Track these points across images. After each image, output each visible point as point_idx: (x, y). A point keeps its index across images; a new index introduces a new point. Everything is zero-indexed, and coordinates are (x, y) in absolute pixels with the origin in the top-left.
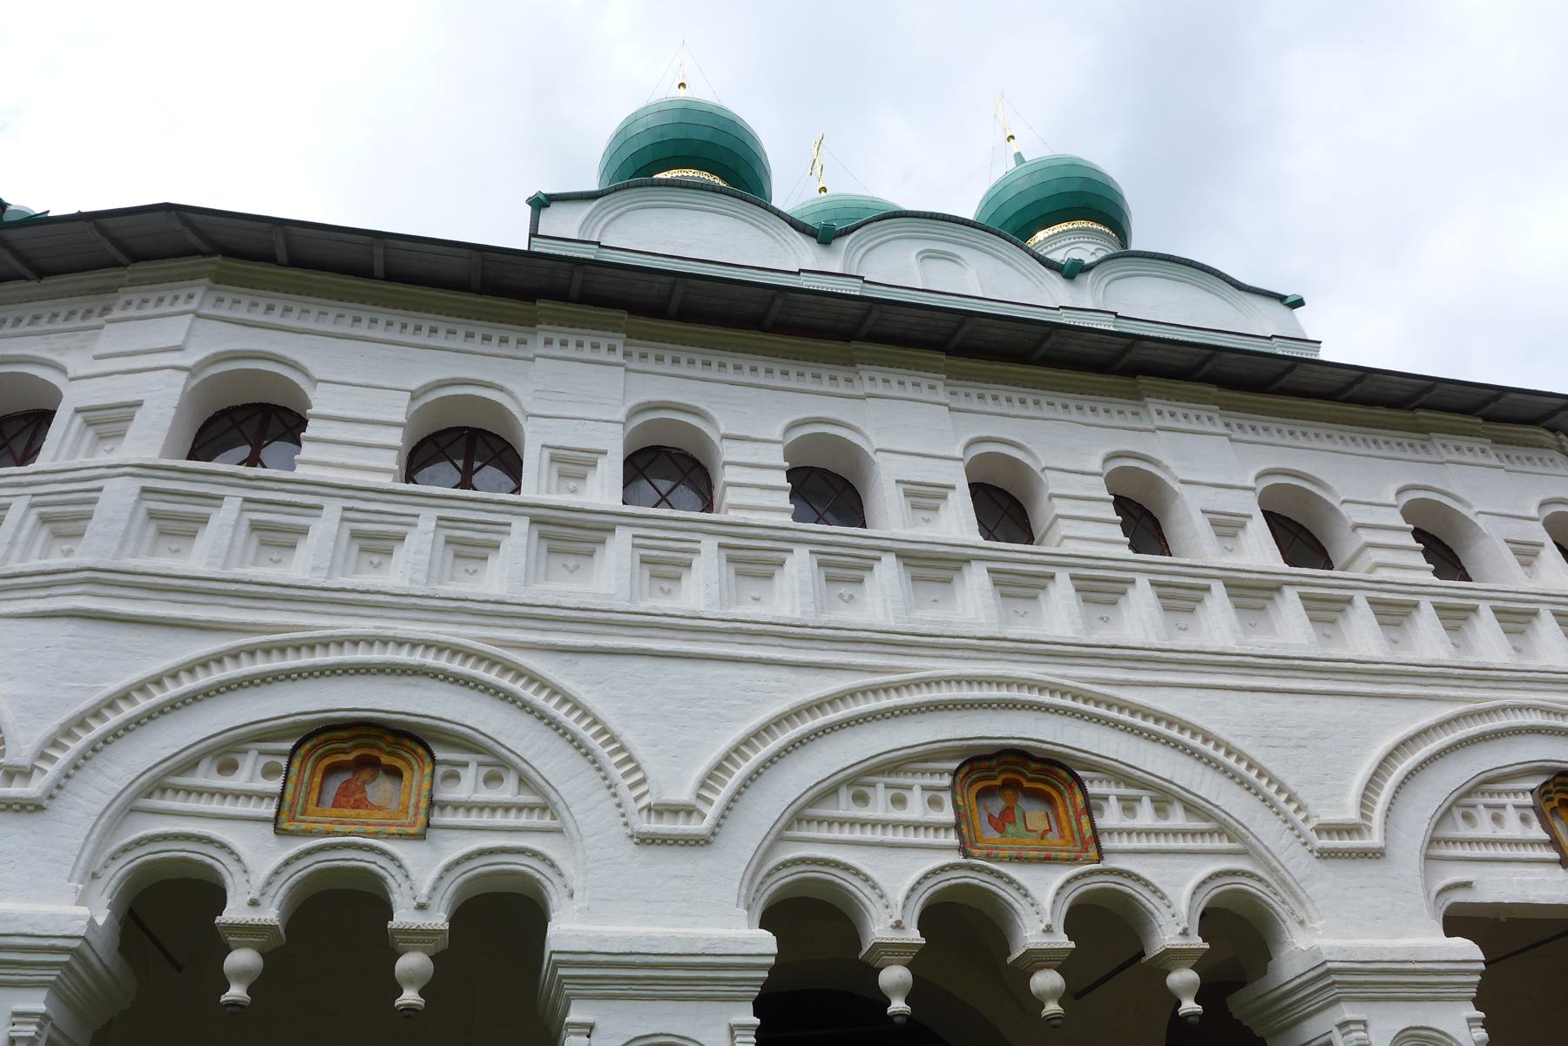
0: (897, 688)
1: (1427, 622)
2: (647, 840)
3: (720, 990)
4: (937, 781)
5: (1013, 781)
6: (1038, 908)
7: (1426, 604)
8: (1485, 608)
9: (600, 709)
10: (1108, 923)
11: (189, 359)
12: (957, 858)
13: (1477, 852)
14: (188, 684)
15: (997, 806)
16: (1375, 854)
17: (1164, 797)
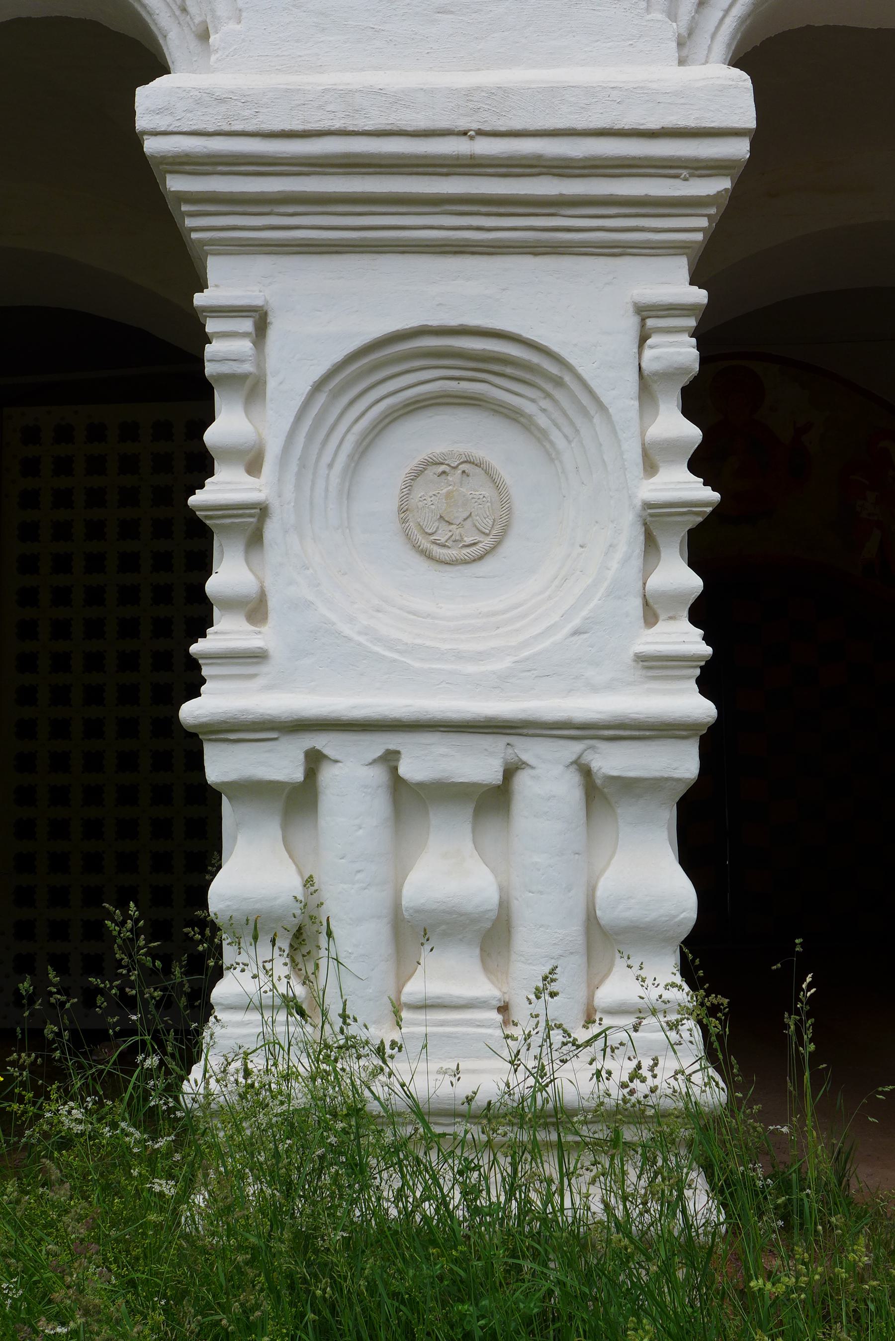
3: (309, 226)
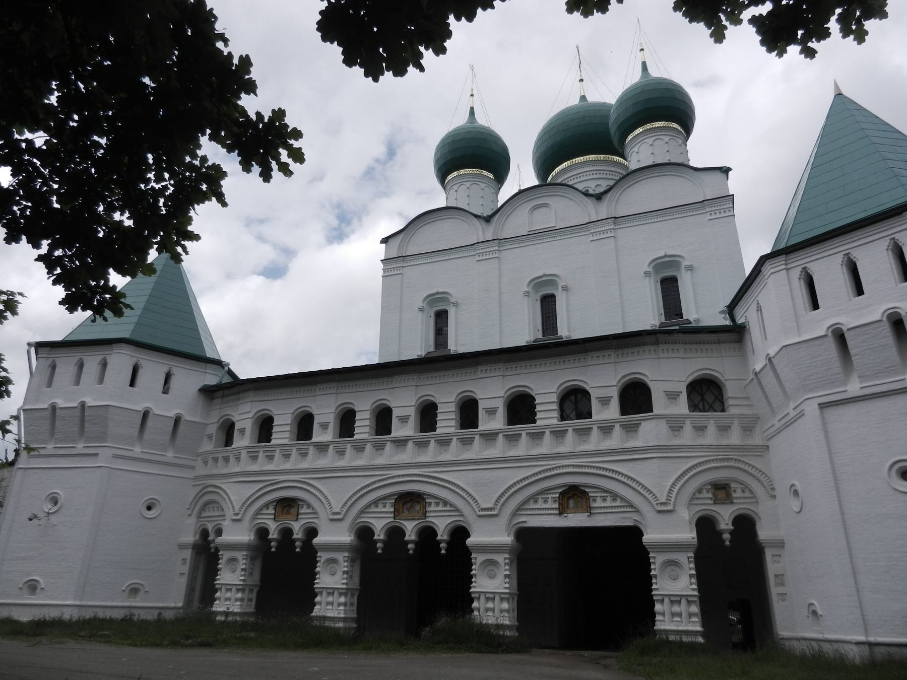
0: (385, 479)
1: (688, 428)
2: (332, 520)
4: (554, 496)
5: (409, 501)
6: (410, 529)
7: (617, 426)
8: (595, 428)
9: (325, 492)
10: (428, 534)
11: (250, 415)
12: (392, 520)
13: (537, 512)
14: (259, 494)
15: (409, 505)
16: (496, 516)
17: (446, 503)
